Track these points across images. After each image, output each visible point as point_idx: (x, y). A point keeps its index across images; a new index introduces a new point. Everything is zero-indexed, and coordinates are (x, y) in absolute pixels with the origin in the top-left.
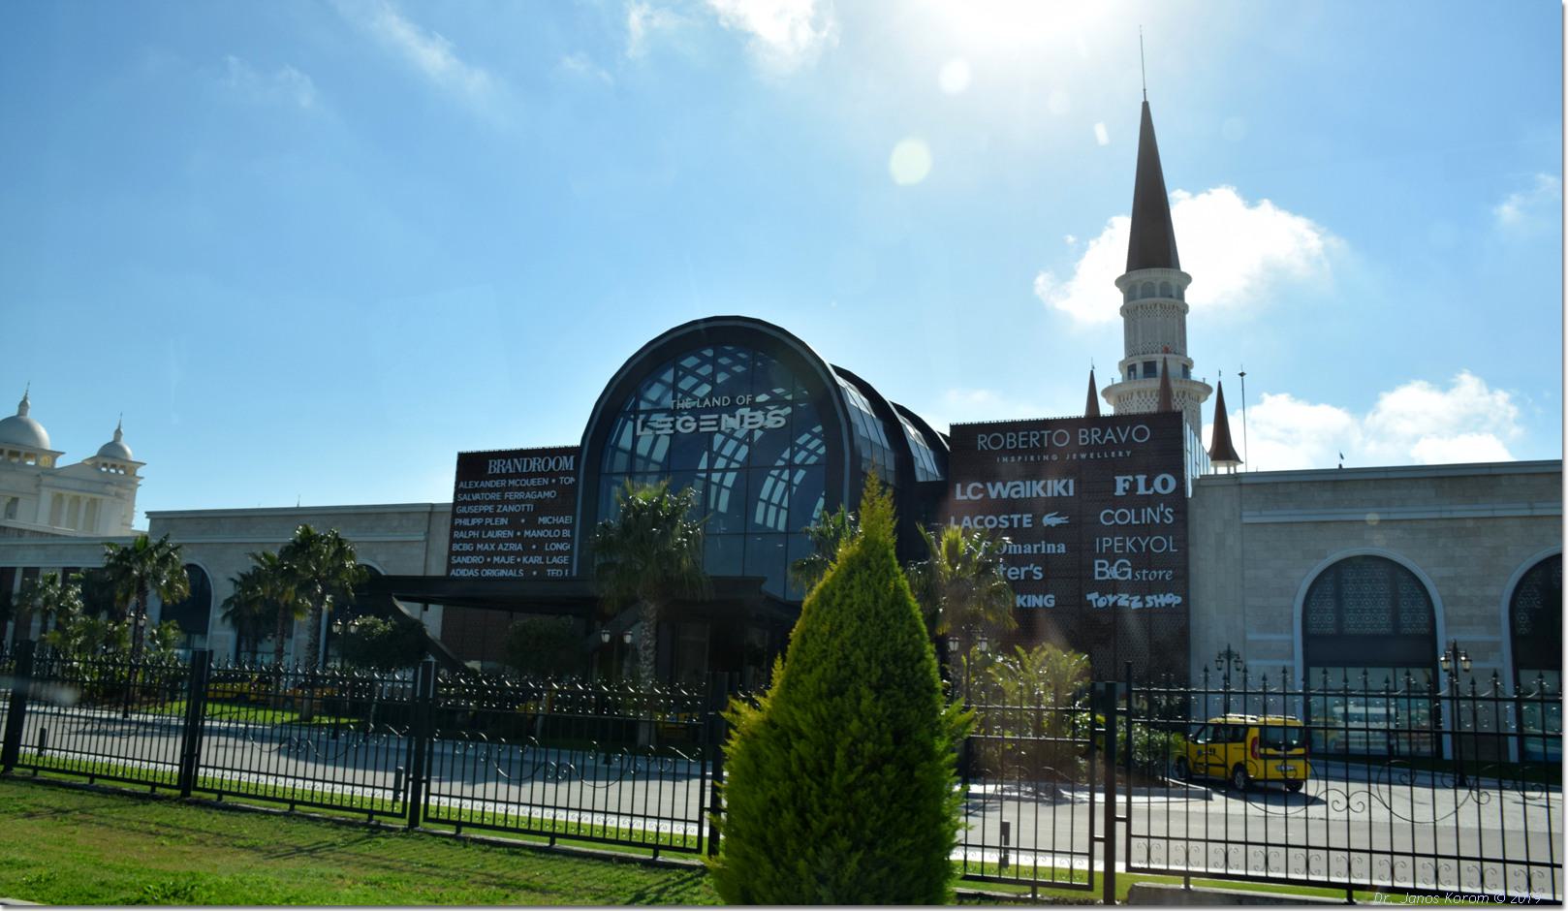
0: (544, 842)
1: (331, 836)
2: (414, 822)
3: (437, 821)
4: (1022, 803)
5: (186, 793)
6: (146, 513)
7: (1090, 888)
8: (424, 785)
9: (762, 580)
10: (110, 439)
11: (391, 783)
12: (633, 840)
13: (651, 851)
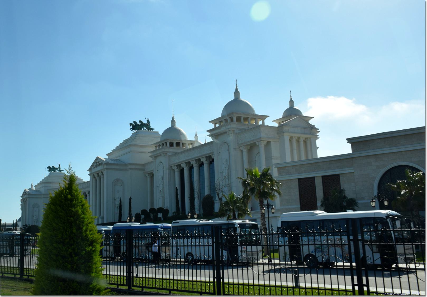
2: (130, 288)
4: (259, 266)
5: (21, 276)
6: (347, 139)
8: (216, 276)
10: (288, 106)
12: (211, 292)
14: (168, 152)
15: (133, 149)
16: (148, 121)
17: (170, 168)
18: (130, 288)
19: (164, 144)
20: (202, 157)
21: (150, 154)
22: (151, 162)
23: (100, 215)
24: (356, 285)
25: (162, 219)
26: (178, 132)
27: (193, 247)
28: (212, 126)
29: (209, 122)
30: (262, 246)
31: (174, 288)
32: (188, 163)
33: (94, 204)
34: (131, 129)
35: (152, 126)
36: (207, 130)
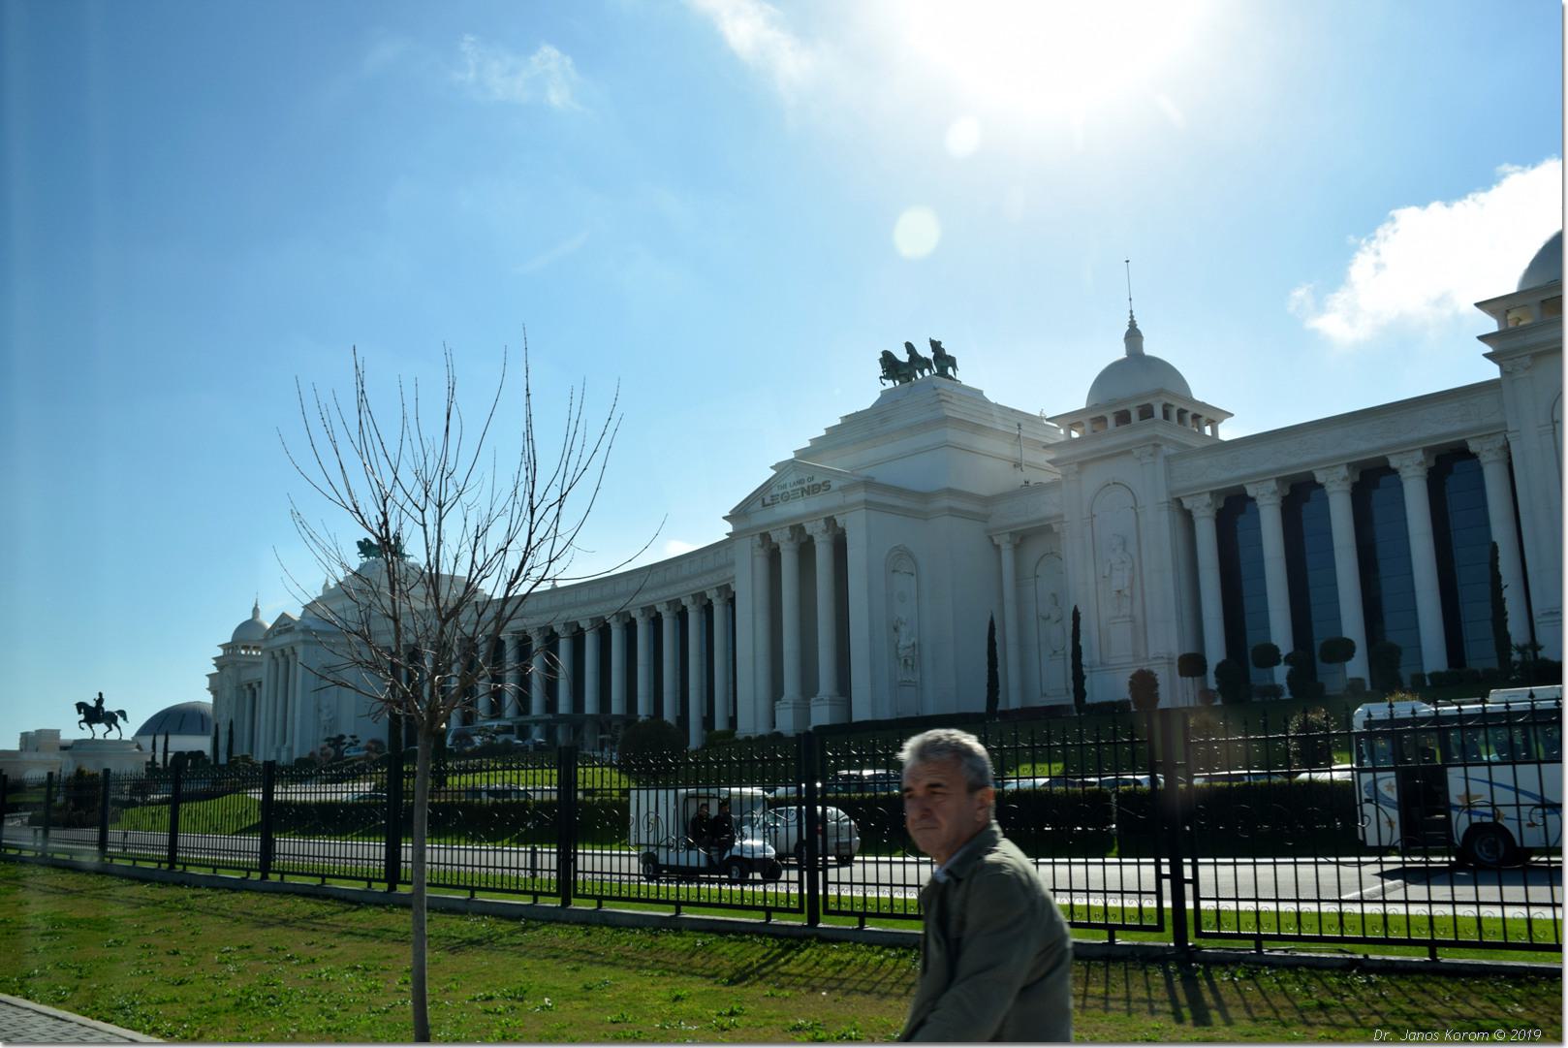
0: (1419, 956)
3: (839, 913)
8: (820, 873)
11: (1149, 884)
12: (868, 911)
13: (673, 907)
14: (238, 662)
15: (952, 435)
17: (239, 688)
19: (1109, 420)
20: (1474, 435)
21: (1052, 456)
22: (1055, 485)
23: (285, 742)
24: (1188, 881)
25: (1132, 705)
28: (220, 652)
30: (719, 798)
32: (699, 596)
33: (270, 717)
34: (881, 378)
36: (215, 656)
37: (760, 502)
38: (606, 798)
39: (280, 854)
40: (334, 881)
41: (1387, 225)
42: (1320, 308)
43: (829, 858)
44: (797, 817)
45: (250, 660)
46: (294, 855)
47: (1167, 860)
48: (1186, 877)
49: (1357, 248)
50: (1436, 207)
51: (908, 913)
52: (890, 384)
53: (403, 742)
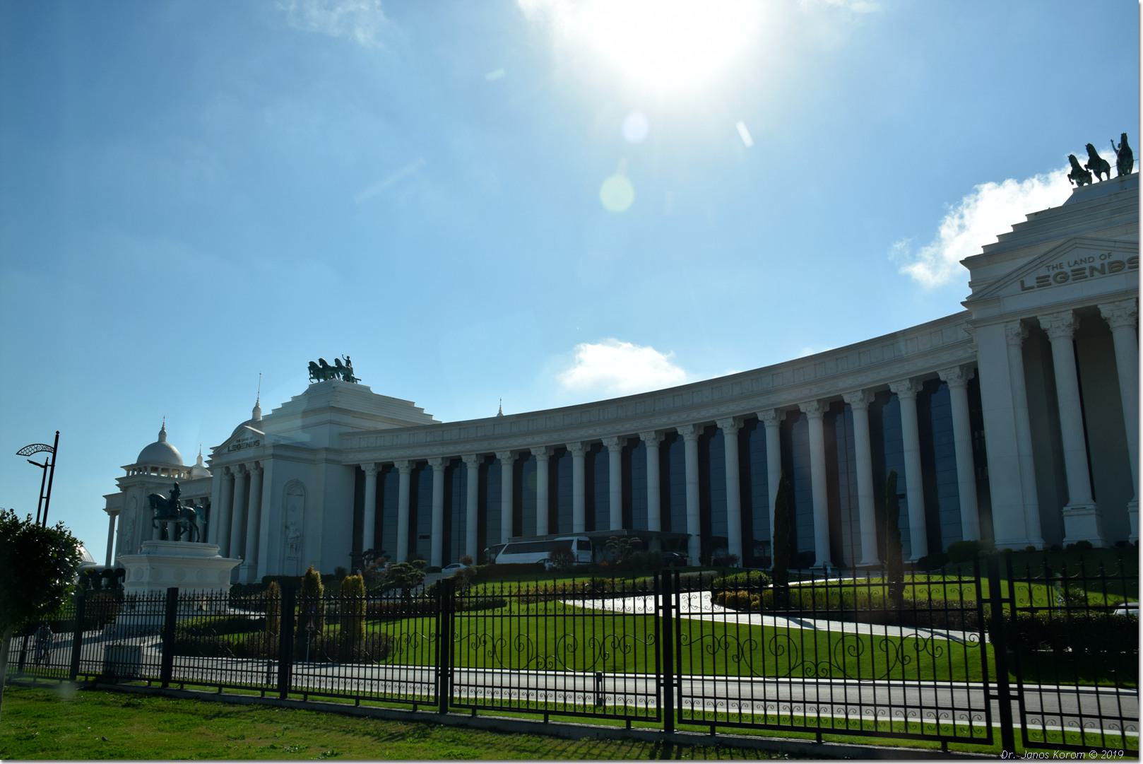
1: (402, 728)
3: (693, 722)
7: (989, 741)
8: (675, 689)
9: (117, 485)
16: (348, 362)
18: (283, 696)
26: (168, 450)
27: (576, 618)
28: (123, 474)
29: (122, 467)
31: (519, 706)
35: (356, 375)
37: (1018, 284)
38: (1059, 613)
39: (176, 666)
40: (367, 702)
41: (972, 195)
42: (914, 258)
43: (991, 685)
44: (436, 639)
45: (159, 481)
46: (96, 661)
47: (996, 685)
48: (997, 701)
49: (946, 212)
50: (1010, 185)
51: (706, 720)
52: (315, 381)
53: (505, 548)
